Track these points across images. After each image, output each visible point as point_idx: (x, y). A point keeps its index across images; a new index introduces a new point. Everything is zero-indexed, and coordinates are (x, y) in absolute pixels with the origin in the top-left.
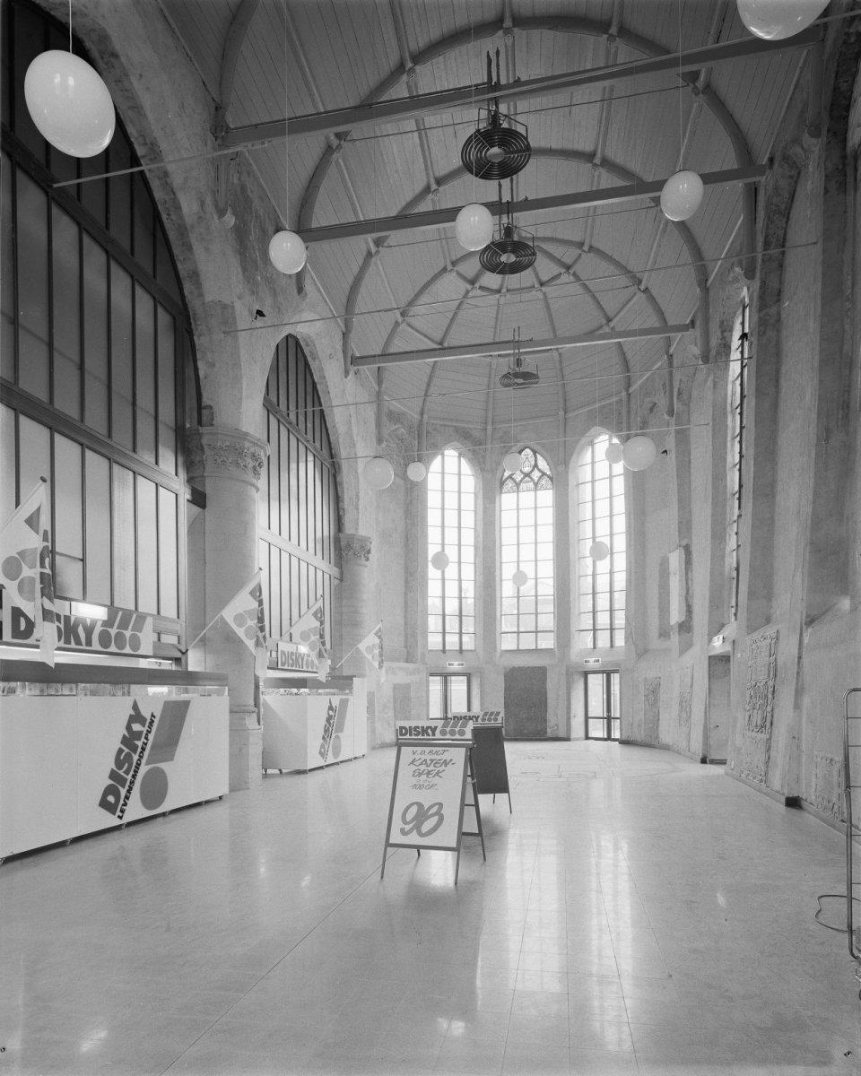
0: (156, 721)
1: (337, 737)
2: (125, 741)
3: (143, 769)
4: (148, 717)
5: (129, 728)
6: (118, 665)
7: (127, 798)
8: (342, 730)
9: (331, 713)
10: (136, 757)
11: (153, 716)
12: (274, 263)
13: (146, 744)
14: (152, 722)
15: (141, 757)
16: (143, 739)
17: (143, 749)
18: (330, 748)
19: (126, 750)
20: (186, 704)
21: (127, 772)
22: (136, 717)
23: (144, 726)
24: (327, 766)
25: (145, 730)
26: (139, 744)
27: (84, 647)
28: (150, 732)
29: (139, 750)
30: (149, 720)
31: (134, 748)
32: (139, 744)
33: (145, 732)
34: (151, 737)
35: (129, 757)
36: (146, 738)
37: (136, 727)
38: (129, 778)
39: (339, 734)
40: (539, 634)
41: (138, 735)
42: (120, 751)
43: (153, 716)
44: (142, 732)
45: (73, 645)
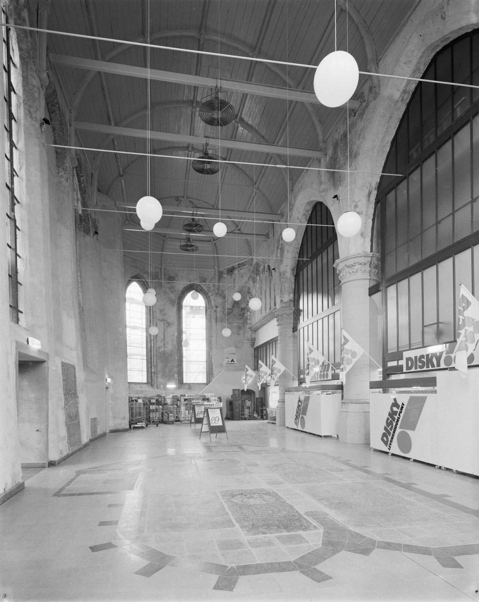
0: (405, 407)
1: (302, 417)
2: (390, 414)
3: (398, 430)
4: (401, 405)
5: (391, 409)
6: (419, 377)
7: (391, 441)
8: (305, 415)
9: (299, 403)
10: (394, 424)
11: (403, 404)
12: (344, 236)
13: (399, 418)
14: (402, 407)
15: (397, 424)
16: (398, 416)
17: (398, 421)
18: (300, 421)
19: (391, 419)
20: (426, 397)
21: (391, 429)
22: (395, 404)
23: (398, 408)
24: (302, 431)
25: (399, 411)
26: (396, 417)
27: (436, 368)
28: (401, 413)
29: (396, 420)
30: (401, 407)
31: (394, 419)
32: (396, 417)
33: (399, 412)
34: (402, 415)
35: (391, 423)
36: (399, 415)
37: (395, 409)
38: (392, 432)
39: (304, 416)
40: (436, 322)
41: (395, 413)
42: (388, 419)
43: (403, 404)
44: (397, 412)
45: (430, 368)
